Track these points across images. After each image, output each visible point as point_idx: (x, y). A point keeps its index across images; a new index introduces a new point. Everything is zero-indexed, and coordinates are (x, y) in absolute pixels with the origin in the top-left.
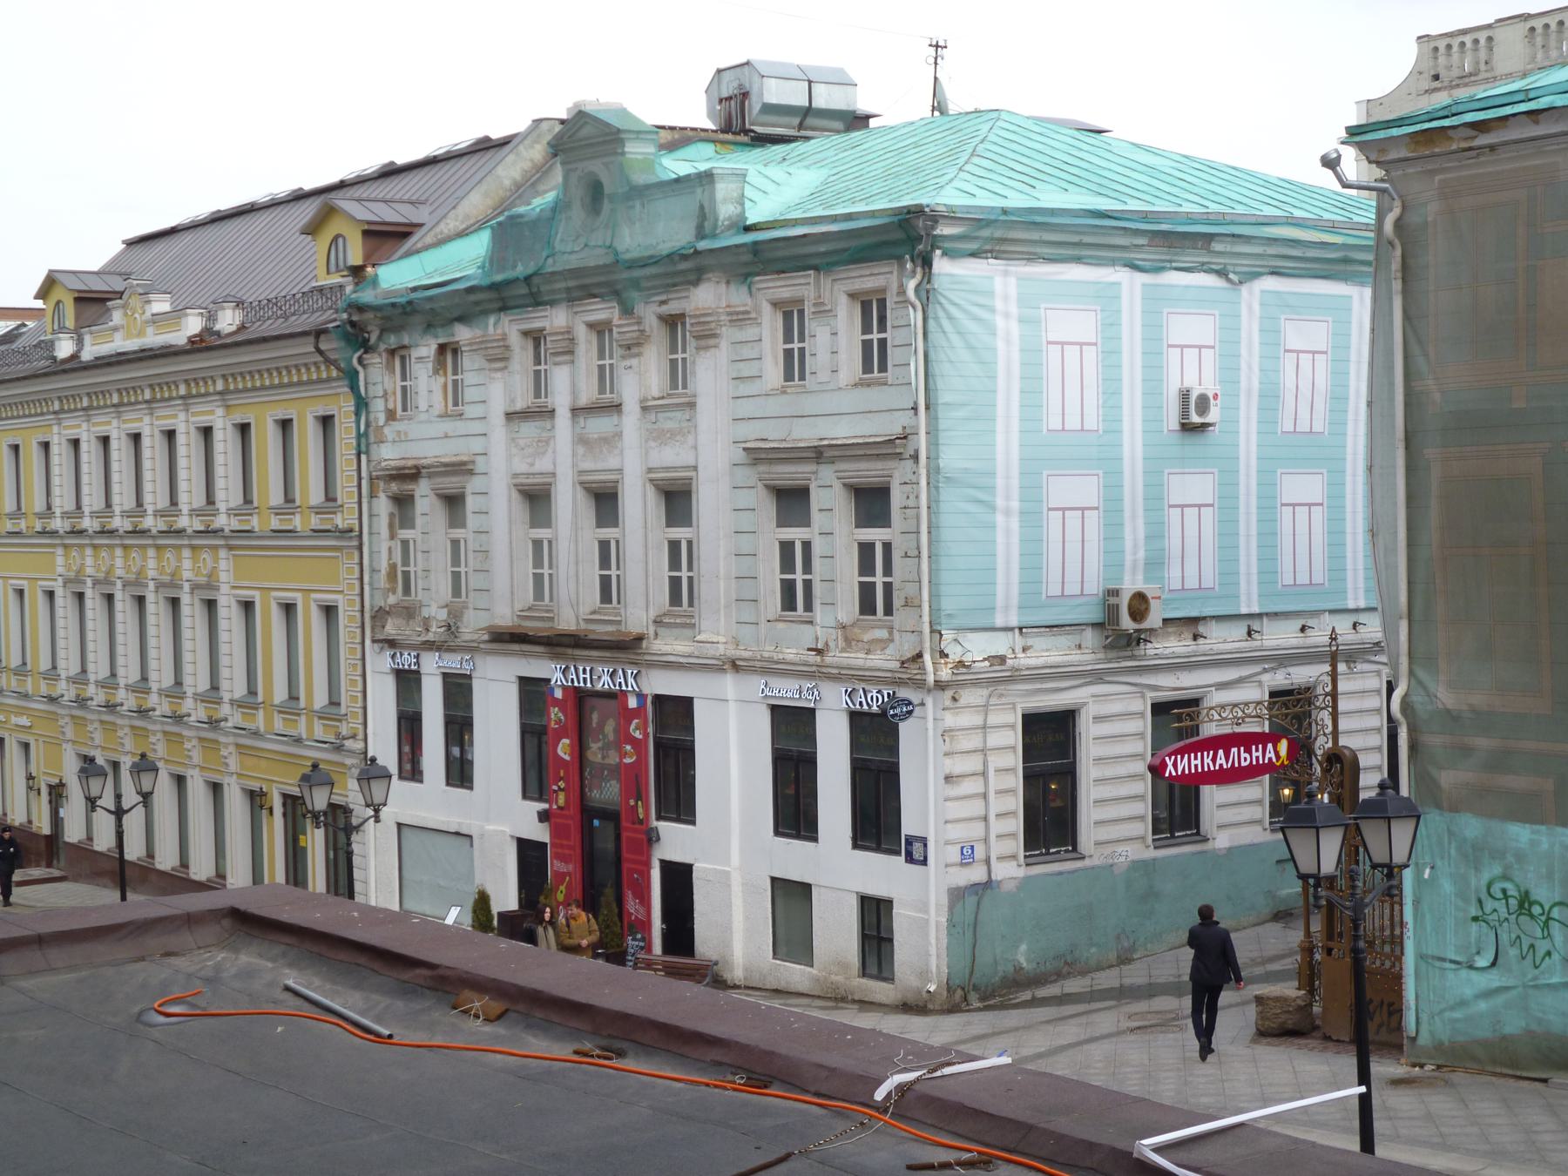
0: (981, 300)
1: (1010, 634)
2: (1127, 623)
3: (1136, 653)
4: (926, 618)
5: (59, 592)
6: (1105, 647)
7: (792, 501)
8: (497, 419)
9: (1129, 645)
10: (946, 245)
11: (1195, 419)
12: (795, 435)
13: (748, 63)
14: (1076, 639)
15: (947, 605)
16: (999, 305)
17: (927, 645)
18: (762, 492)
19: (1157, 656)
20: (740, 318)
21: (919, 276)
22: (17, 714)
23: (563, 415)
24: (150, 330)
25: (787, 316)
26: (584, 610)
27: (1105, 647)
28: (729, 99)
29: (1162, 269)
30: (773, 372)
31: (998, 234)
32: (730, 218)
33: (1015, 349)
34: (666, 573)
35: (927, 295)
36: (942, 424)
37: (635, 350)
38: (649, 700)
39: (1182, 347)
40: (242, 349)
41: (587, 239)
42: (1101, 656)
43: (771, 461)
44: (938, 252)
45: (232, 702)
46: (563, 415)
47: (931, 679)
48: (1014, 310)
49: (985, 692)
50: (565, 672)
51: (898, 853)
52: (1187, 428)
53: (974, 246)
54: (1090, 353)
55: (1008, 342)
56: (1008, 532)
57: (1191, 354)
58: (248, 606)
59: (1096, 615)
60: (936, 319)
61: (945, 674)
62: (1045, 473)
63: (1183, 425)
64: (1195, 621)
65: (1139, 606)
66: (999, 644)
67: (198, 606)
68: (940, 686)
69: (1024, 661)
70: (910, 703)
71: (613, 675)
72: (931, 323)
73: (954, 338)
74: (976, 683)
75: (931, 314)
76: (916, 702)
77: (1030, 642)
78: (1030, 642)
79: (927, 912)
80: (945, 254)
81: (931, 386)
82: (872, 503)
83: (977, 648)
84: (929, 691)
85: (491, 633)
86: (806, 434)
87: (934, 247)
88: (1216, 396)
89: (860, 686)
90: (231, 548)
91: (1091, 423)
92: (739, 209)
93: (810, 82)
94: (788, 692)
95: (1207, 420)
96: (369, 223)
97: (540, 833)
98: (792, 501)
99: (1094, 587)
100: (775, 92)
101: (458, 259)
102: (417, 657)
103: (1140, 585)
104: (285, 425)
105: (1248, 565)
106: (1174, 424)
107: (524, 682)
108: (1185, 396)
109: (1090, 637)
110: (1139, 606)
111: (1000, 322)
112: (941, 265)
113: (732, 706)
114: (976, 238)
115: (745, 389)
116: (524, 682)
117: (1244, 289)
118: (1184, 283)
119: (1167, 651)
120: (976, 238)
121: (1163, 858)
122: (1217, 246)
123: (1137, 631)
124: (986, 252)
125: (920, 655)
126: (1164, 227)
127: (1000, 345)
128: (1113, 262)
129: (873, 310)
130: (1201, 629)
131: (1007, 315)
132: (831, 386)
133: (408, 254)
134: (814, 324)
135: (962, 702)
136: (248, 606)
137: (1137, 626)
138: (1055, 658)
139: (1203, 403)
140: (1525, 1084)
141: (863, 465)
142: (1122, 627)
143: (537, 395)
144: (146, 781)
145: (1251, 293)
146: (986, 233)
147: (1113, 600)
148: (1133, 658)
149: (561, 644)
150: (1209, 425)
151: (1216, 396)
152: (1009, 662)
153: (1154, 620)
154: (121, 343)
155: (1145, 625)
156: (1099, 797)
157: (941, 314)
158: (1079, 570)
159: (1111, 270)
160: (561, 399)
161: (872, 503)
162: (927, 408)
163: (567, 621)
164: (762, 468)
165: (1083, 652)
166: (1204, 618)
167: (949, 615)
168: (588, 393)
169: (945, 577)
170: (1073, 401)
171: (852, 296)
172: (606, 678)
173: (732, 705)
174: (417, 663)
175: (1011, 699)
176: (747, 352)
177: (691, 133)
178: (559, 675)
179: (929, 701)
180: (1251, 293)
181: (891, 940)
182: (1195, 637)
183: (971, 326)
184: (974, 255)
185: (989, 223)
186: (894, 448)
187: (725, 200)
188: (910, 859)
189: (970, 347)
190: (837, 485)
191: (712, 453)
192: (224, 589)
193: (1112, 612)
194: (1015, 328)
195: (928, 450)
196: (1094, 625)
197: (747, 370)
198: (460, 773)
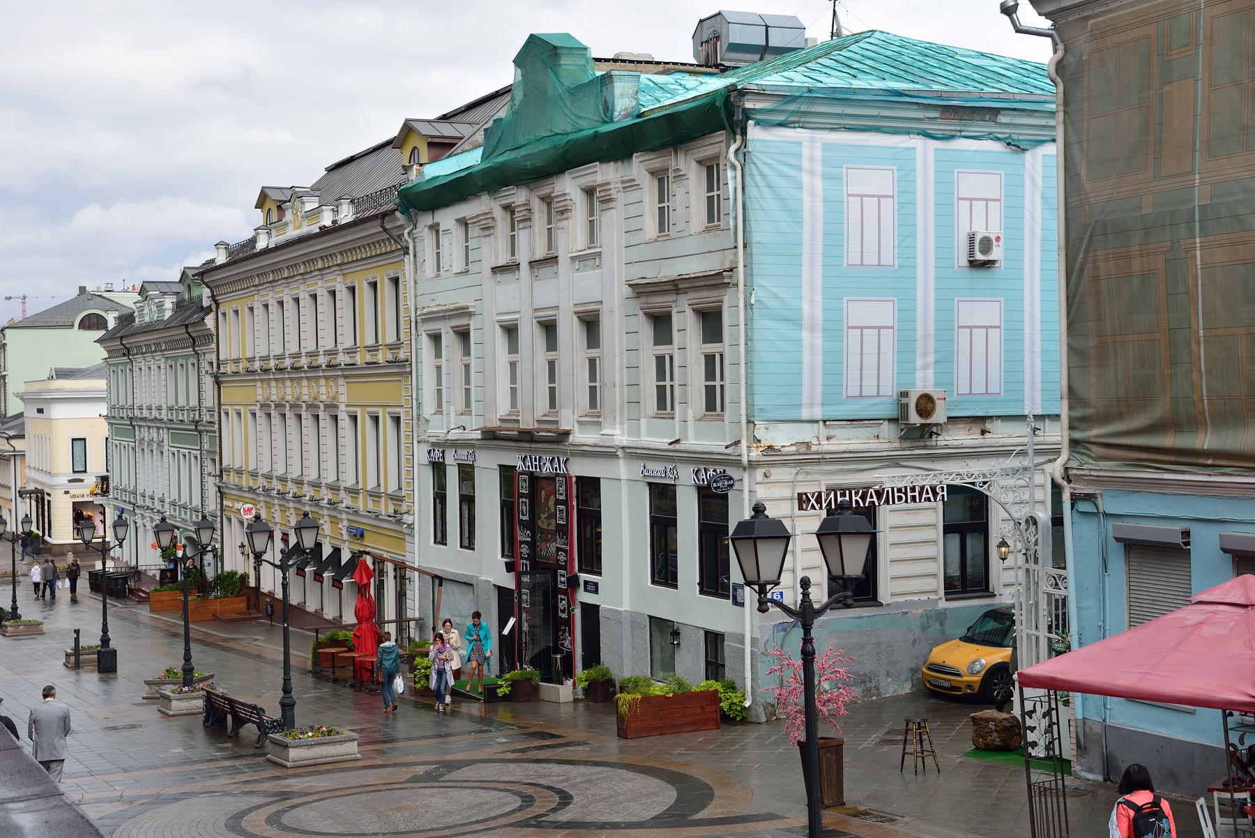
0: (793, 161)
1: (815, 425)
2: (915, 418)
3: (929, 443)
4: (743, 412)
5: (258, 413)
6: (901, 438)
7: (661, 324)
8: (487, 272)
9: (922, 437)
10: (759, 117)
11: (979, 256)
12: (662, 274)
13: (719, 14)
14: (874, 431)
15: (759, 401)
16: (805, 164)
17: (744, 432)
18: (642, 318)
19: (947, 447)
20: (629, 185)
21: (739, 142)
22: (239, 501)
23: (524, 266)
24: (306, 223)
25: (661, 181)
26: (539, 414)
27: (901, 438)
28: (707, 42)
29: (952, 137)
30: (650, 227)
31: (803, 108)
32: (626, 109)
33: (819, 200)
34: (587, 384)
35: (743, 153)
36: (756, 259)
37: (565, 216)
38: (574, 480)
39: (971, 200)
40: (346, 232)
41: (553, 136)
42: (897, 445)
43: (648, 294)
44: (751, 122)
45: (346, 489)
46: (524, 266)
47: (745, 460)
48: (818, 168)
49: (794, 471)
50: (524, 460)
51: (727, 597)
52: (974, 264)
53: (781, 118)
54: (887, 204)
55: (813, 194)
56: (812, 347)
57: (979, 207)
58: (354, 418)
59: (892, 412)
60: (751, 175)
61: (755, 454)
62: (845, 299)
63: (971, 262)
64: (983, 419)
65: (926, 404)
66: (806, 433)
67: (328, 418)
68: (753, 465)
69: (827, 446)
70: (731, 478)
71: (552, 461)
72: (748, 178)
73: (766, 192)
74: (785, 464)
75: (747, 172)
76: (735, 478)
77: (832, 432)
78: (832, 432)
79: (743, 643)
80: (757, 123)
81: (748, 229)
82: (711, 322)
83: (783, 437)
84: (745, 469)
85: (483, 432)
86: (670, 271)
87: (748, 118)
88: (998, 239)
89: (702, 467)
90: (345, 377)
91: (887, 259)
92: (634, 103)
93: (767, 27)
94: (657, 469)
95: (991, 258)
96: (432, 137)
97: (509, 581)
98: (661, 324)
99: (890, 389)
100: (737, 36)
101: (469, 159)
102: (443, 452)
103: (930, 389)
104: (374, 285)
105: (1033, 375)
106: (964, 261)
107: (503, 468)
108: (972, 238)
109: (887, 430)
110: (926, 404)
111: (806, 178)
112: (754, 132)
113: (624, 484)
114: (783, 111)
115: (634, 239)
116: (503, 468)
117: (1028, 155)
118: (974, 148)
119: (956, 443)
120: (783, 111)
121: (953, 609)
122: (1003, 119)
123: (922, 425)
124: (794, 122)
125: (739, 442)
126: (953, 103)
127: (806, 198)
128: (907, 132)
129: (712, 169)
130: (988, 426)
131: (812, 173)
132: (685, 234)
133: (450, 156)
134: (675, 186)
135: (773, 478)
136: (354, 418)
137: (924, 421)
138: (855, 445)
139: (986, 244)
140: (339, 799)
141: (705, 294)
142: (916, 424)
143: (513, 254)
144: (121, 531)
145: (1034, 158)
146: (793, 107)
147: (904, 400)
148: (925, 447)
149: (527, 437)
150: (993, 262)
151: (998, 239)
152: (814, 448)
153: (939, 416)
154: (292, 233)
155: (932, 420)
156: (895, 557)
157: (755, 171)
158: (878, 378)
159: (906, 137)
160: (523, 258)
161: (711, 322)
162: (745, 246)
163: (527, 423)
164: (643, 300)
165: (885, 440)
166: (991, 417)
167: (761, 410)
168: (540, 253)
169: (757, 379)
170: (872, 239)
171: (700, 162)
172: (548, 464)
173: (624, 484)
174: (443, 457)
175: (815, 477)
176: (633, 210)
177: (671, 66)
178: (520, 463)
179: (746, 477)
180: (1034, 158)
181: (723, 666)
182: (983, 432)
183: (777, 180)
184: (781, 125)
185: (794, 99)
186: (719, 281)
187: (622, 96)
188: (736, 603)
189: (780, 199)
190: (689, 311)
191: (606, 285)
192: (342, 407)
193: (904, 408)
194: (819, 184)
195: (745, 279)
196: (890, 420)
197: (633, 224)
198: (468, 541)
